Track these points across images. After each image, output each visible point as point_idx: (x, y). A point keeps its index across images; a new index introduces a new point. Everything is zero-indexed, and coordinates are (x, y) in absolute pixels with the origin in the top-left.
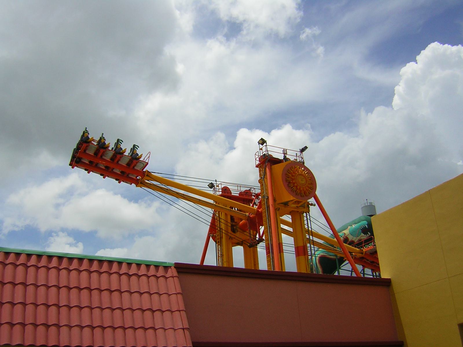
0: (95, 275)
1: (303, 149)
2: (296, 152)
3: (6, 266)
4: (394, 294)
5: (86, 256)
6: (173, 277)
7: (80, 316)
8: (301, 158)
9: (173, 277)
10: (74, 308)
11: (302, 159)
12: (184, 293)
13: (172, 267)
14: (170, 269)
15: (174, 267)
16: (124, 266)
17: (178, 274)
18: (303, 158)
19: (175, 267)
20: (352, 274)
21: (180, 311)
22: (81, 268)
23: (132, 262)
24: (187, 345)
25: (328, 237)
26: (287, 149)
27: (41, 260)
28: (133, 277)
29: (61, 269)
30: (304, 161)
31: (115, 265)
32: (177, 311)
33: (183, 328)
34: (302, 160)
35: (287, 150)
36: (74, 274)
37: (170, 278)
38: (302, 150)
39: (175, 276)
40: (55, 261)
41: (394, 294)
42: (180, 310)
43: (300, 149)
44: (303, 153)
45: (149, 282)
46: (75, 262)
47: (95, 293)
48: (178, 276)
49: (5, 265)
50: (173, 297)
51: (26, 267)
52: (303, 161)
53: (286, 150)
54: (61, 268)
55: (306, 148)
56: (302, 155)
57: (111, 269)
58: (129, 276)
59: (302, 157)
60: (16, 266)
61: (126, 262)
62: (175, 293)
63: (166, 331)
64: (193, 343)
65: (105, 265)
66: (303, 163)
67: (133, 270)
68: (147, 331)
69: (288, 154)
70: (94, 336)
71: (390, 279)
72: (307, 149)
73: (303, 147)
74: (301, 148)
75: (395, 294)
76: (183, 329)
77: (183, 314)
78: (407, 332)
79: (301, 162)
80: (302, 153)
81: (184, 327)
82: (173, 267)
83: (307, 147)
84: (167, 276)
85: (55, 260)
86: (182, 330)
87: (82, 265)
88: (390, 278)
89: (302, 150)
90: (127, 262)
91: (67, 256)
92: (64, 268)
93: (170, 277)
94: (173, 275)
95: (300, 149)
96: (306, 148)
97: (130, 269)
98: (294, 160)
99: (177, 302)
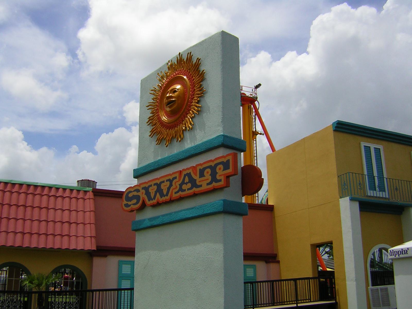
0: (30, 197)
1: (257, 86)
2: (252, 89)
3: (12, 194)
4: (274, 218)
5: (25, 182)
6: (89, 199)
7: (16, 225)
8: (255, 93)
9: (89, 199)
10: (12, 219)
11: (255, 95)
12: (96, 212)
13: (90, 192)
14: (88, 193)
15: (91, 192)
16: (53, 190)
17: (94, 197)
18: (256, 94)
19: (92, 192)
20: (269, 202)
21: (91, 224)
22: (21, 190)
23: (60, 187)
24: (92, 248)
25: (137, 168)
26: (242, 86)
27: (79, 193)
28: (59, 198)
29: (6, 192)
30: (257, 96)
31: (46, 189)
32: (88, 223)
33: (90, 236)
34: (256, 96)
35: (243, 87)
36: (15, 195)
37: (87, 199)
38: (257, 87)
39: (91, 199)
40: (68, 192)
41: (275, 217)
42: (91, 223)
43: (254, 86)
44: (257, 89)
45: (70, 202)
46: (17, 186)
47: (29, 209)
48: (94, 198)
49: (4, 192)
50: (88, 213)
51: (27, 194)
52: (257, 96)
53: (242, 87)
54: (6, 190)
55: (260, 85)
56: (256, 91)
57: (43, 192)
58: (56, 197)
59: (256, 93)
60: (19, 193)
61: (55, 187)
62: (89, 210)
63: (78, 238)
64: (97, 247)
65: (39, 189)
66: (257, 98)
67: (60, 193)
68: (63, 237)
69: (243, 90)
70: (24, 239)
71: (273, 205)
72: (261, 86)
73: (257, 84)
74: (255, 85)
75: (276, 218)
76: (91, 237)
77: (93, 226)
78: (279, 247)
79: (254, 97)
80: (256, 90)
81: (92, 236)
82: (91, 192)
83: (261, 84)
84: (86, 198)
85: (17, 186)
86: (89, 238)
87: (22, 188)
88: (273, 204)
89: (257, 87)
90: (84, 190)
91: (11, 182)
92: (8, 191)
93: (87, 199)
94: (90, 197)
95: (254, 86)
96: (260, 85)
97: (71, 194)
98: (250, 96)
99: (90, 217)
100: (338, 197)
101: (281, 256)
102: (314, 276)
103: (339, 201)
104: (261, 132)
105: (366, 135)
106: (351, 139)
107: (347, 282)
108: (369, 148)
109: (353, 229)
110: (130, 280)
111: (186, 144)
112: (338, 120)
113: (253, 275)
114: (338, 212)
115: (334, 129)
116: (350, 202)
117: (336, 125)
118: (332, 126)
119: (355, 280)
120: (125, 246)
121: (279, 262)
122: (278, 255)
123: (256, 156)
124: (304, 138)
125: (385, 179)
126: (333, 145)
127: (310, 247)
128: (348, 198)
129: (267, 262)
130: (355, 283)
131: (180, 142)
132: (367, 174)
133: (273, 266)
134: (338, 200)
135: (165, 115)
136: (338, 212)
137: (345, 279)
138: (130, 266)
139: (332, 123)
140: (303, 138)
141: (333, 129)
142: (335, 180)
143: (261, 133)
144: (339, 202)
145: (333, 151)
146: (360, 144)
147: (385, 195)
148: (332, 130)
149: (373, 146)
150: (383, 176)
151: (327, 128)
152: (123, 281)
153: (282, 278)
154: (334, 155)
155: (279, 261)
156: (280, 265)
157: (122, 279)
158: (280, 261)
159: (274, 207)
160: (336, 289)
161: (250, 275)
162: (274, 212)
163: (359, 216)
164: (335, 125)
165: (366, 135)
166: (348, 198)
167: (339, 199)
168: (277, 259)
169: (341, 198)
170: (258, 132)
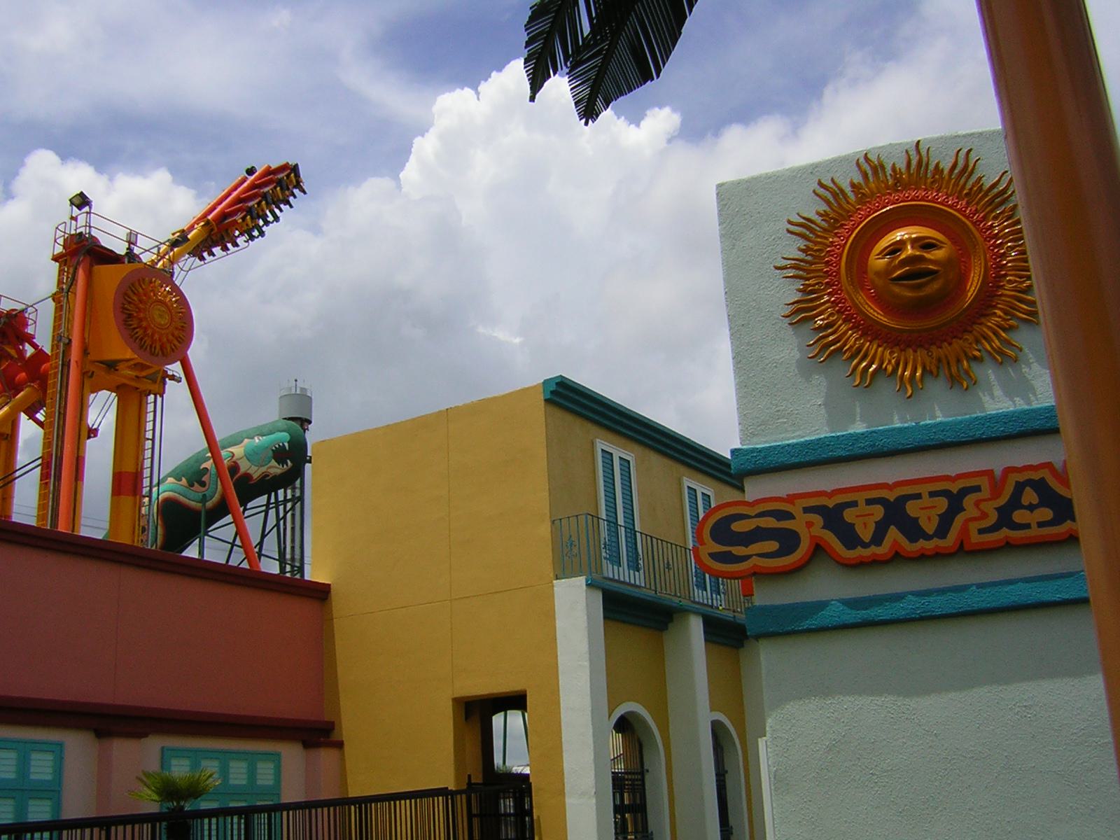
26: (138, 233)
71: (329, 585)
75: (335, 620)
100: (552, 575)
101: (349, 728)
102: (459, 788)
103: (553, 586)
104: (175, 374)
105: (606, 422)
106: (580, 430)
107: (568, 801)
108: (609, 456)
109: (591, 661)
110: (14, 798)
111: (986, 398)
112: (561, 376)
113: (49, 777)
114: (549, 615)
115: (548, 397)
116: (586, 590)
117: (555, 386)
118: (542, 390)
119: (595, 793)
120: (16, 693)
121: (339, 745)
122: (336, 727)
123: (151, 437)
124: (447, 409)
125: (638, 535)
126: (542, 438)
127: (451, 703)
128: (581, 581)
129: (307, 745)
130: (594, 801)
131: (952, 390)
132: (623, 525)
133: (326, 756)
134: (552, 582)
135: (870, 304)
136: (550, 615)
137: (562, 793)
138: (50, 757)
139: (542, 381)
140: (443, 408)
141: (544, 396)
142: (545, 530)
143: (173, 375)
144: (553, 590)
145: (542, 452)
146: (593, 443)
147: (638, 578)
148: (541, 398)
149: (620, 451)
150: (634, 525)
151: (524, 391)
152: (31, 802)
153: (350, 793)
154: (544, 463)
155: (343, 741)
156: (343, 754)
157: (30, 798)
158: (345, 742)
159: (332, 590)
160: (535, 817)
161: (267, 783)
162: (331, 603)
163: (602, 629)
164: (553, 388)
165: (606, 422)
166: (581, 581)
167: (555, 582)
168: (335, 737)
169: (557, 579)
170: (167, 372)
